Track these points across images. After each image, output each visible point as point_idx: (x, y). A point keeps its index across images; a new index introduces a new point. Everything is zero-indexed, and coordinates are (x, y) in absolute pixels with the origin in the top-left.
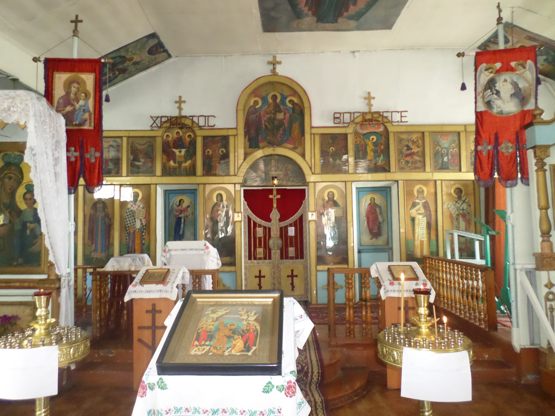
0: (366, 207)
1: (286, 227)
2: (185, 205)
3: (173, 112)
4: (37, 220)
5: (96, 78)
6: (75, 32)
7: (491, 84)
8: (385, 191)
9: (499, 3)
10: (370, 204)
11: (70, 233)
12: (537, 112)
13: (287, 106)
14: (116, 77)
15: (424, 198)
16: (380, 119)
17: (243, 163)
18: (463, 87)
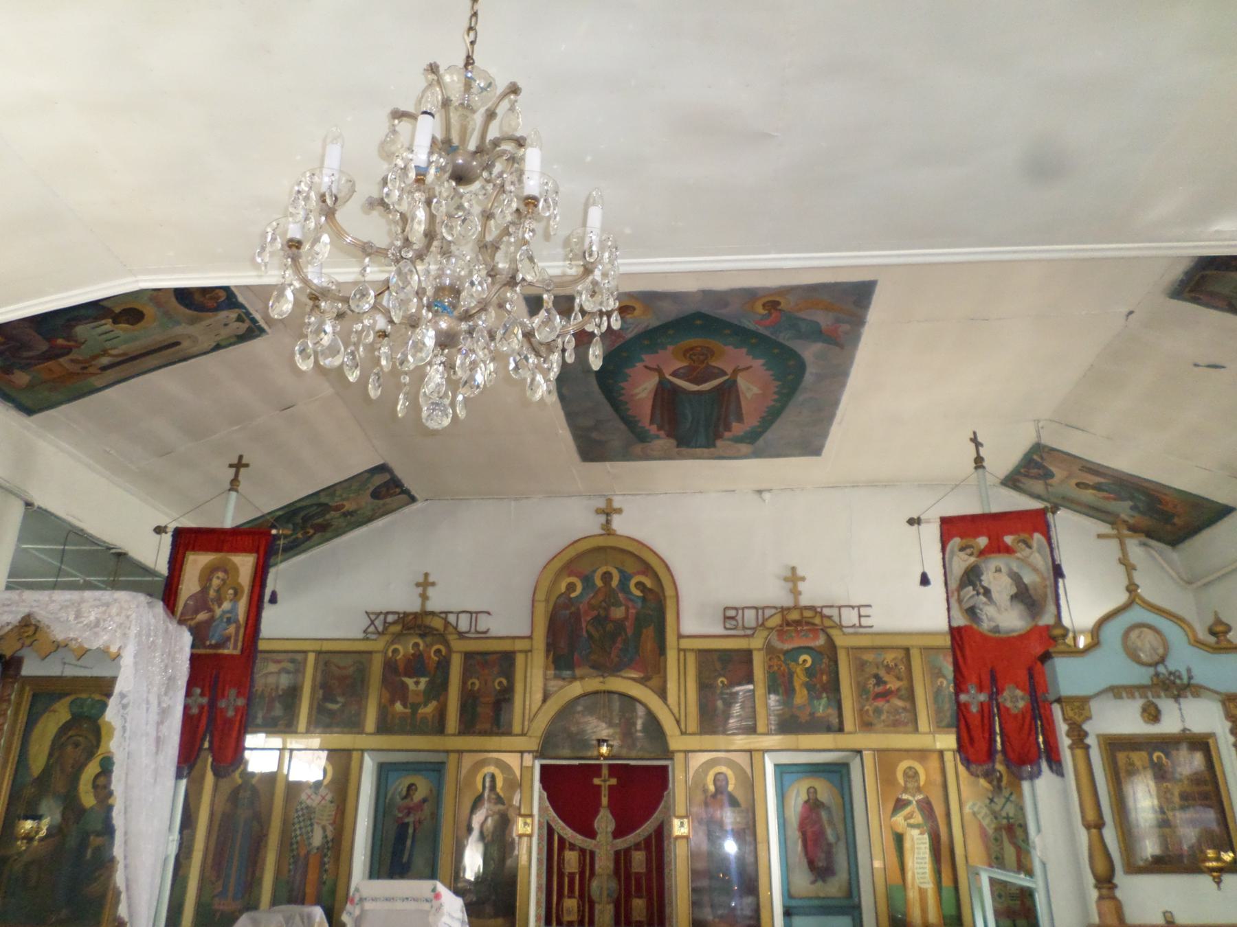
0: (799, 808)
1: (627, 851)
2: (418, 796)
3: (411, 604)
4: (108, 830)
5: (257, 563)
6: (234, 484)
7: (971, 577)
8: (837, 772)
9: (975, 433)
10: (806, 802)
11: (166, 859)
12: (1057, 632)
13: (631, 593)
14: (309, 538)
15: (919, 790)
16: (817, 621)
17: (539, 709)
18: (925, 580)
